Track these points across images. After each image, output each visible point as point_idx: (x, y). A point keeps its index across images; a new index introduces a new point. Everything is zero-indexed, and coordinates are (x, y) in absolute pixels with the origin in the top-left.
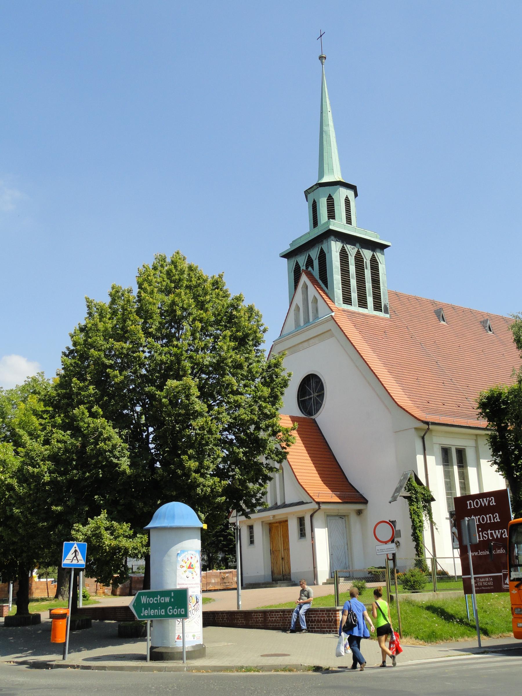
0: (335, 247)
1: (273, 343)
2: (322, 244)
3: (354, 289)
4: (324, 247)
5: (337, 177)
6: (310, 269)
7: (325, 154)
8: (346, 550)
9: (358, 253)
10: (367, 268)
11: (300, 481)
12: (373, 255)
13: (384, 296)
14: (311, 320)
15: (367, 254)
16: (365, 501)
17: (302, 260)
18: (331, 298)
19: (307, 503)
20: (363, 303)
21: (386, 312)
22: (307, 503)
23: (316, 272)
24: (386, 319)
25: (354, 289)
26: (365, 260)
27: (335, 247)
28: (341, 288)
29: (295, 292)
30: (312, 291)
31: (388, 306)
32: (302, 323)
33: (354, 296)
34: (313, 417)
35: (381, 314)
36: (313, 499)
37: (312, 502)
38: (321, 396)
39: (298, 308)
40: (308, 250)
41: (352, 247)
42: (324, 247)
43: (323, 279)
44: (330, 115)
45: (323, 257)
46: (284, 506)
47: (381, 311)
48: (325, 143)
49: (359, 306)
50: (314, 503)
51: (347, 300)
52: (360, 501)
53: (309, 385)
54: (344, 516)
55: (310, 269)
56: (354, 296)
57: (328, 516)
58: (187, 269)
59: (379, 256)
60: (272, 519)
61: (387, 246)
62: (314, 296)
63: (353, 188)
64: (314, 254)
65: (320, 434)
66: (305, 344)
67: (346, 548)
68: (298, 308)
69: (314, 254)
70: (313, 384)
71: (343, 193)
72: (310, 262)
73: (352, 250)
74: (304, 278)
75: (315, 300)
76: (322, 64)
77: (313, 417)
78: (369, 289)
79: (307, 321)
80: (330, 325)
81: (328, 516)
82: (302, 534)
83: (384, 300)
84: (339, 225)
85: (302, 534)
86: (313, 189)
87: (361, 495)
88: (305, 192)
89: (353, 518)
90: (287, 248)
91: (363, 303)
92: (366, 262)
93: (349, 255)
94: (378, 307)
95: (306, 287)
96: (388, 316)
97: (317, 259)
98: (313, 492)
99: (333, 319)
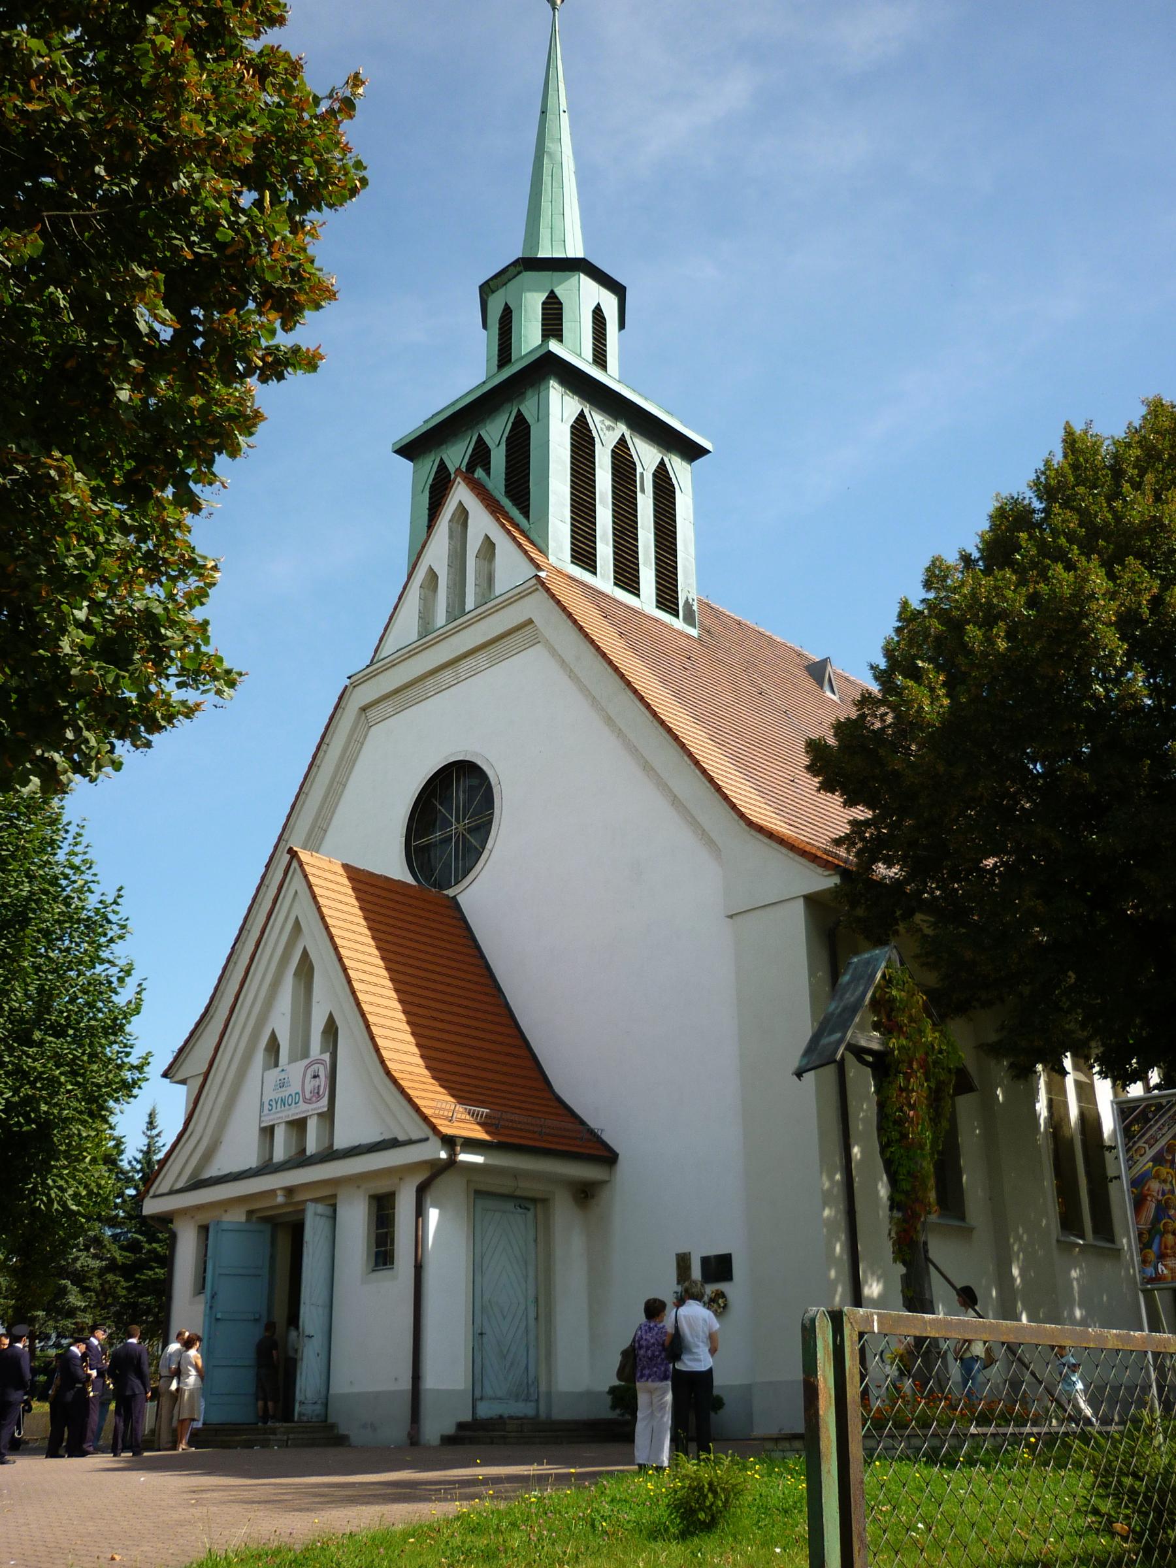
0: (561, 408)
1: (348, 682)
2: (521, 402)
3: (605, 534)
4: (528, 408)
5: (575, 250)
6: (479, 473)
7: (545, 205)
8: (532, 1322)
9: (622, 441)
10: (643, 491)
11: (390, 1064)
12: (662, 463)
13: (686, 577)
14: (470, 604)
15: (647, 456)
16: (608, 1157)
17: (456, 455)
18: (542, 545)
19: (410, 1142)
20: (627, 577)
21: (690, 619)
22: (410, 1142)
23: (496, 479)
24: (688, 637)
25: (605, 534)
26: (639, 470)
27: (561, 408)
28: (568, 520)
29: (428, 537)
30: (481, 523)
31: (695, 608)
32: (441, 618)
33: (605, 550)
34: (451, 892)
35: (678, 624)
36: (434, 1128)
37: (427, 1139)
38: (482, 827)
39: (432, 576)
40: (477, 424)
41: (608, 423)
42: (528, 408)
43: (519, 494)
44: (565, 119)
45: (522, 444)
46: (330, 1155)
47: (677, 616)
48: (546, 178)
49: (615, 584)
50: (435, 1142)
51: (584, 555)
52: (592, 1152)
53: (446, 800)
54: (534, 1200)
55: (479, 473)
56: (605, 550)
57: (479, 1194)
58: (149, 737)
59: (680, 471)
60: (280, 1199)
61: (703, 452)
62: (487, 537)
63: (619, 290)
64: (495, 432)
65: (470, 943)
66: (447, 676)
67: (532, 1315)
68: (432, 576)
69: (495, 432)
70: (459, 794)
71: (584, 295)
72: (481, 456)
73: (607, 433)
74: (461, 494)
75: (489, 547)
76: (554, 9)
77: (451, 892)
78: (646, 547)
79: (457, 609)
80: (534, 607)
81: (479, 1194)
82: (382, 1254)
83: (687, 587)
84: (575, 349)
85: (382, 1254)
86: (504, 278)
87: (591, 1132)
88: (481, 287)
89: (563, 1211)
90: (412, 423)
91: (627, 577)
92: (642, 474)
93: (597, 440)
94: (667, 598)
95: (462, 514)
96: (694, 632)
97: (503, 446)
98: (433, 1104)
99: (543, 584)
